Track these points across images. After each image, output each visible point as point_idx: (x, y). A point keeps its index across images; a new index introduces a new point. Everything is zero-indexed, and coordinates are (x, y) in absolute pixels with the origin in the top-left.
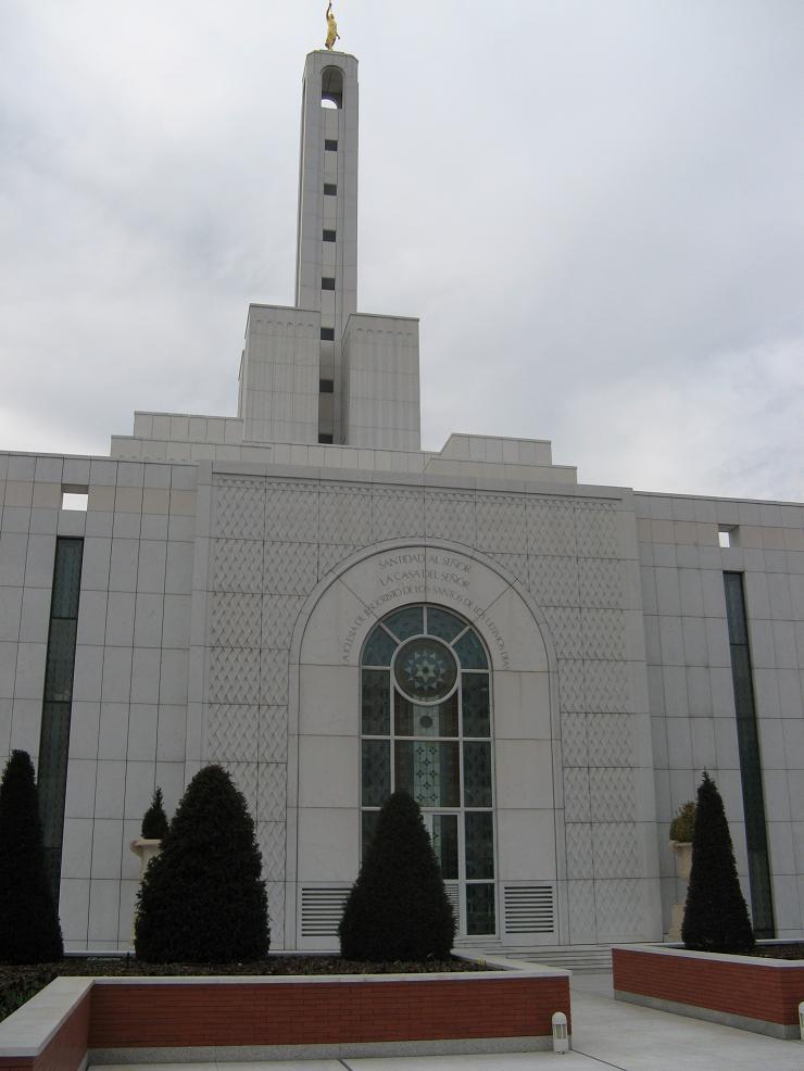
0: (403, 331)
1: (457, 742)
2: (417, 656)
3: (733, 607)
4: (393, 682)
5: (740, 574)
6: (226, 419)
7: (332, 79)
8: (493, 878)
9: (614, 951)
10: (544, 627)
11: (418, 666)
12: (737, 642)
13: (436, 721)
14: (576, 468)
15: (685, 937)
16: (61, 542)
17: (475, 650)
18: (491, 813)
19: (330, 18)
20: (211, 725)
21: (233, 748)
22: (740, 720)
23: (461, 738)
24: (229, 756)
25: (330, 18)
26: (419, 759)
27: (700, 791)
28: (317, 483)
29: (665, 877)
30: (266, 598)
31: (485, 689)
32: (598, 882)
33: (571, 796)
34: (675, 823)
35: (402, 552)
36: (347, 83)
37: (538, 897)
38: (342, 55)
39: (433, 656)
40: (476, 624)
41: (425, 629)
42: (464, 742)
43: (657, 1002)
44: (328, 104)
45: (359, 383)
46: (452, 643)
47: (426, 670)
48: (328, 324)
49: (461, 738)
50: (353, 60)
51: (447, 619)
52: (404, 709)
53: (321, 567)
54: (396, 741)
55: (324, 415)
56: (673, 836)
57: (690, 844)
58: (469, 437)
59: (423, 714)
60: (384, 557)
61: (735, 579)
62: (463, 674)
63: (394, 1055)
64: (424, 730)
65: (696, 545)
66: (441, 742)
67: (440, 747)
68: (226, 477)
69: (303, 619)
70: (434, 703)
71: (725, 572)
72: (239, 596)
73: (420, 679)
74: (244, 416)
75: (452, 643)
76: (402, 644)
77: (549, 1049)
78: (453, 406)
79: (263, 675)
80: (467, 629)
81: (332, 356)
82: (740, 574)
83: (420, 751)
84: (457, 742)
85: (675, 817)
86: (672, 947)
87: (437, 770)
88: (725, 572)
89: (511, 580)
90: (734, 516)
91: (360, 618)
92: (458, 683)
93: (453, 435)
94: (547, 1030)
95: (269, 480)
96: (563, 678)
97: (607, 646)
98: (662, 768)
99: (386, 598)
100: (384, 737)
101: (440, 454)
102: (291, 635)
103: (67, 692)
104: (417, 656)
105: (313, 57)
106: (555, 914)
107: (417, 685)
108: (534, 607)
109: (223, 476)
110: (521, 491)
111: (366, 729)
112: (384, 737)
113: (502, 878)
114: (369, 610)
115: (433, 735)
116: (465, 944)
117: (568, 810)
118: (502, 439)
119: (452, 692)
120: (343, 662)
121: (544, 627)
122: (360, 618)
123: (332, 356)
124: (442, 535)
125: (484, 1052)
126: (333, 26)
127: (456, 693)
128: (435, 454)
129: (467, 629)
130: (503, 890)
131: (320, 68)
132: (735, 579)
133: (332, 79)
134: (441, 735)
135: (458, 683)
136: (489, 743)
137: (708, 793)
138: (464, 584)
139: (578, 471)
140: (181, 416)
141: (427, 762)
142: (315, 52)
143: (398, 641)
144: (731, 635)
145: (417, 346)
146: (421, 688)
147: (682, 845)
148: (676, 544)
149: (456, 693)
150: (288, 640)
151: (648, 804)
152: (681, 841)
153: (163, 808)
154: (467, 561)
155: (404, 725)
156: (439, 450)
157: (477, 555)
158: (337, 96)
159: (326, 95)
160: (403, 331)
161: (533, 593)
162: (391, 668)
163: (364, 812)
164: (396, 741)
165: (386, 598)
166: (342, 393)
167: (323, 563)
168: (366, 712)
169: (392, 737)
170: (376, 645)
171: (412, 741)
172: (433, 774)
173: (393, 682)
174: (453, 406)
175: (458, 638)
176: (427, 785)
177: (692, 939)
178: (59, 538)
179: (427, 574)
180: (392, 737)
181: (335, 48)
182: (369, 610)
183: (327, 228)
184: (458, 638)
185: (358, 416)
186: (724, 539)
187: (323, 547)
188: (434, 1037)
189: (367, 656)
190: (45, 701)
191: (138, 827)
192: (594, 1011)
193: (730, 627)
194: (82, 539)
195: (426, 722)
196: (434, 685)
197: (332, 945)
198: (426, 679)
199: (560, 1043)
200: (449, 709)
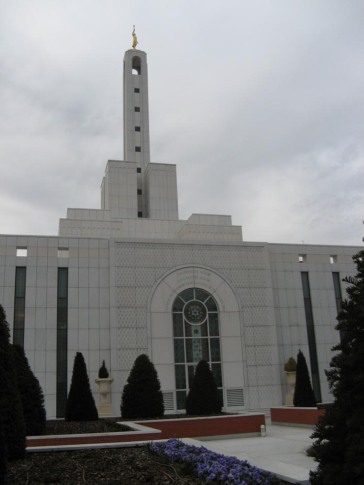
0: (170, 170)
1: (208, 339)
2: (192, 307)
5: (307, 273)
6: (97, 210)
7: (136, 61)
8: (222, 387)
9: (271, 409)
10: (237, 295)
12: (306, 298)
13: (200, 331)
14: (241, 227)
15: (294, 404)
16: (57, 266)
17: (213, 306)
18: (220, 364)
19: (134, 35)
20: (119, 336)
21: (142, 344)
22: (308, 327)
23: (209, 337)
24: (141, 347)
25: (134, 35)
26: (194, 345)
27: (298, 356)
28: (153, 244)
29: (284, 384)
30: (137, 288)
31: (217, 319)
32: (259, 387)
33: (249, 356)
34: (286, 365)
35: (186, 269)
36: (142, 64)
37: (238, 395)
38: (139, 51)
39: (198, 307)
40: (213, 295)
41: (195, 297)
43: (287, 424)
44: (135, 72)
45: (153, 192)
46: (205, 302)
47: (195, 313)
48: (139, 166)
49: (209, 337)
50: (144, 54)
51: (203, 294)
52: (188, 327)
53: (156, 277)
55: (140, 205)
56: (286, 369)
57: (295, 372)
58: (199, 215)
59: (195, 329)
60: (179, 271)
61: (305, 275)
62: (209, 314)
63: (216, 440)
64: (195, 334)
65: (291, 262)
66: (202, 339)
68: (120, 244)
69: (151, 295)
70: (198, 325)
72: (130, 288)
73: (193, 316)
74: (107, 208)
75: (205, 302)
76: (186, 303)
77: (260, 436)
78: (190, 202)
79: (137, 316)
80: (210, 297)
81: (141, 182)
82: (307, 273)
85: (286, 362)
86: (290, 405)
87: (201, 349)
89: (225, 278)
90: (304, 251)
91: (171, 295)
93: (193, 214)
94: (259, 430)
95: (136, 244)
96: (245, 314)
97: (257, 301)
98: (281, 345)
99: (179, 287)
100: (182, 338)
101: (187, 221)
102: (146, 301)
103: (65, 326)
104: (192, 307)
105: (128, 53)
106: (244, 401)
108: (233, 288)
109: (119, 243)
110: (219, 238)
111: (175, 335)
112: (182, 338)
113: (226, 386)
114: (174, 291)
116: (226, 408)
117: (248, 362)
118: (206, 215)
119: (206, 320)
120: (166, 311)
121: (237, 295)
122: (171, 295)
123: (141, 182)
124: (199, 262)
125: (241, 438)
126: (135, 39)
128: (185, 221)
129: (210, 297)
130: (226, 391)
131: (131, 57)
132: (305, 275)
133: (136, 61)
134: (202, 336)
137: (301, 356)
138: (208, 281)
139: (336, 317)
140: (86, 209)
141: (197, 346)
142: (129, 50)
143: (185, 302)
145: (176, 176)
146: (194, 319)
147: (289, 372)
148: (284, 262)
150: (146, 304)
151: (274, 359)
152: (289, 371)
153: (106, 367)
154: (208, 272)
155: (188, 333)
156: (187, 219)
157: (212, 270)
158: (138, 68)
159: (134, 67)
160: (170, 170)
161: (233, 283)
162: (183, 312)
163: (176, 365)
165: (179, 287)
166: (145, 195)
167: (157, 274)
168: (175, 328)
170: (177, 305)
172: (199, 350)
174: (190, 202)
175: (206, 300)
176: (197, 355)
177: (296, 403)
178: (59, 268)
179: (194, 277)
180: (185, 338)
181: (137, 48)
182: (174, 291)
183: (137, 126)
184: (206, 300)
185: (153, 206)
186: (301, 259)
187: (156, 269)
188: (227, 434)
189: (174, 309)
190: (58, 329)
191: (97, 374)
192: (269, 427)
193: (303, 291)
194: (67, 268)
195: (196, 331)
197: (184, 411)
198: (195, 316)
199: (263, 434)
200: (204, 327)
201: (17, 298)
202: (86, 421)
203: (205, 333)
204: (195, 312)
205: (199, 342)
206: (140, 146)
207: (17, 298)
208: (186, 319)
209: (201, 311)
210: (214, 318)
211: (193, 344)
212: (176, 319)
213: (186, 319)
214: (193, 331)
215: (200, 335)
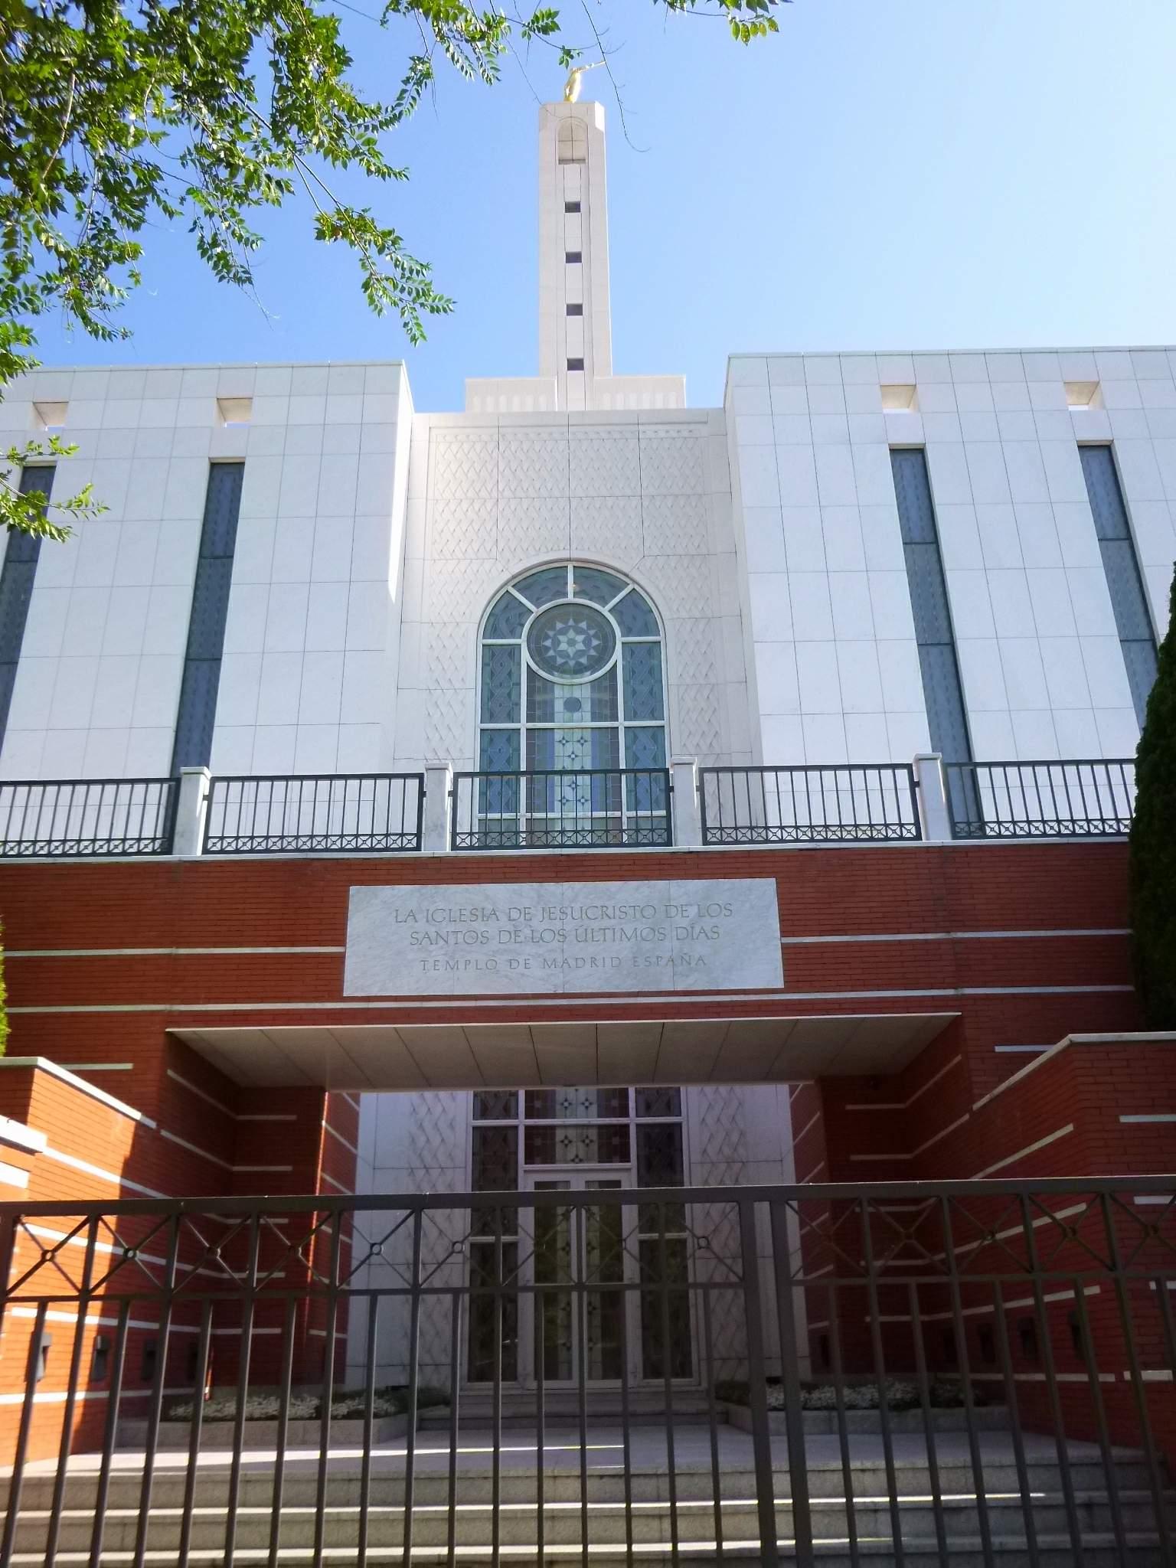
2: (559, 625)
3: (1105, 511)
4: (525, 656)
11: (561, 638)
12: (1110, 534)
17: (638, 613)
42: (638, 1125)
47: (572, 643)
54: (527, 1128)
59: (568, 695)
64: (568, 715)
66: (600, 1127)
67: (600, 1136)
71: (1082, 447)
83: (567, 1142)
84: (627, 1126)
88: (1082, 447)
92: (618, 655)
104: (559, 625)
107: (560, 661)
111: (488, 714)
115: (585, 720)
127: (615, 665)
135: (618, 655)
136: (680, 1125)
144: (1121, 627)
149: (615, 665)
162: (522, 641)
164: (527, 1128)
169: (522, 1122)
171: (553, 1128)
173: (525, 656)
180: (522, 1122)
195: (573, 705)
196: (584, 660)
201: (272, 1418)
202: (117, 1302)
203: (605, 708)
204: (571, 643)
205: (582, 741)
206: (580, 356)
207: (272, 1418)
208: (1042, 1059)
209: (576, 621)
210: (646, 663)
211: (558, 748)
212: (497, 664)
213: (1042, 1059)
214: (559, 706)
215: (588, 716)
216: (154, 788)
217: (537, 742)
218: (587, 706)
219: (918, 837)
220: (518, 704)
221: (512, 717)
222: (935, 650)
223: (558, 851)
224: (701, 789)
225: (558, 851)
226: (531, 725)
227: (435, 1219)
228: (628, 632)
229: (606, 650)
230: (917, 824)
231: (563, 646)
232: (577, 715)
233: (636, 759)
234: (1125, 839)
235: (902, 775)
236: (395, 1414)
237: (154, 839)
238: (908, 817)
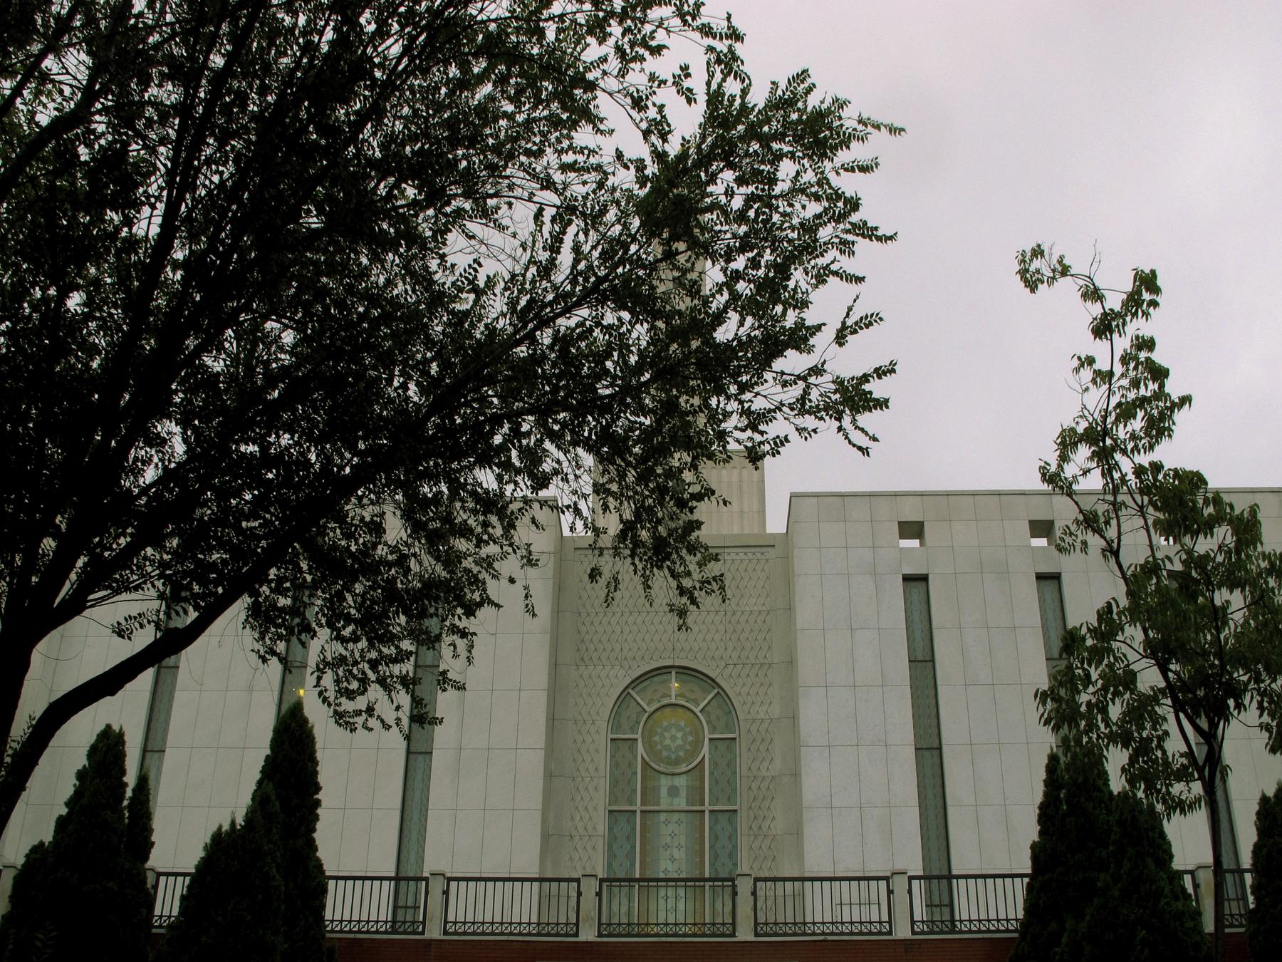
2: (657, 738)
47: (673, 738)
107: (665, 754)
162: (638, 736)
211: (663, 827)
216: (386, 883)
217: (649, 823)
218: (683, 793)
219: (890, 933)
220: (635, 791)
221: (631, 801)
222: (927, 754)
223: (664, 939)
224: (754, 893)
225: (664, 939)
226: (644, 808)
227: (946, 910)
228: (713, 729)
229: (697, 745)
230: (890, 922)
231: (668, 742)
232: (676, 801)
233: (730, 821)
234: (1016, 935)
235: (883, 884)
236: (865, 378)
237: (386, 922)
238: (885, 918)
